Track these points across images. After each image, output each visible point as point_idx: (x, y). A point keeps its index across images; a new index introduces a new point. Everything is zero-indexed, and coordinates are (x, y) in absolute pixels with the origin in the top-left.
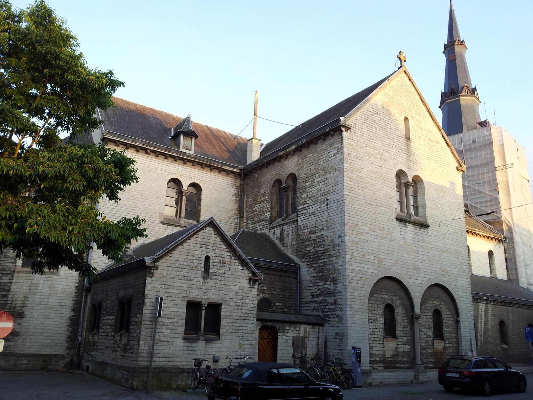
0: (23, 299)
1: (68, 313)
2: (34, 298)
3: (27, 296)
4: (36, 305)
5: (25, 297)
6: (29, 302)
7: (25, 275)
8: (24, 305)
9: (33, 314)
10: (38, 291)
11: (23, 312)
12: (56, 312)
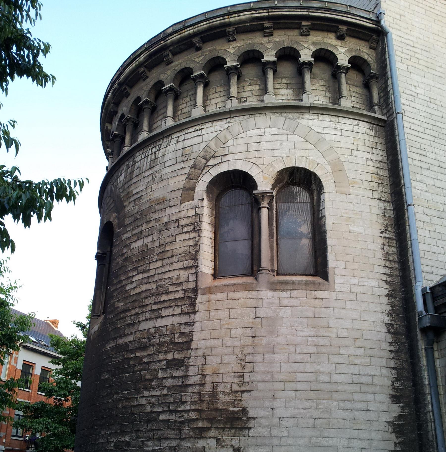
0: (237, 368)
1: (385, 407)
2: (271, 362)
3: (249, 358)
4: (280, 386)
5: (243, 362)
6: (257, 377)
7: (231, 295)
8: (243, 387)
9: (279, 412)
10: (280, 340)
11: (244, 411)
12: (349, 405)
